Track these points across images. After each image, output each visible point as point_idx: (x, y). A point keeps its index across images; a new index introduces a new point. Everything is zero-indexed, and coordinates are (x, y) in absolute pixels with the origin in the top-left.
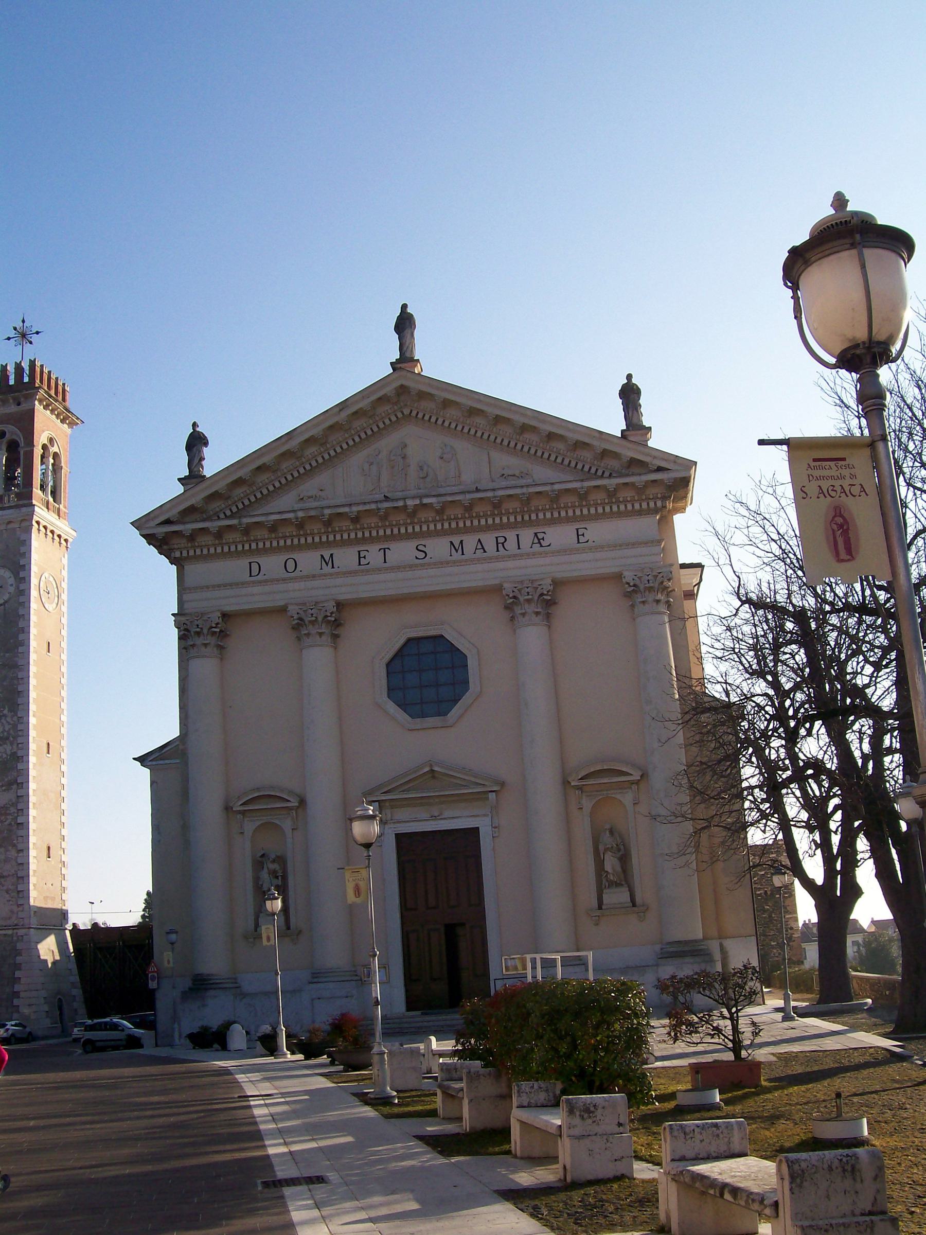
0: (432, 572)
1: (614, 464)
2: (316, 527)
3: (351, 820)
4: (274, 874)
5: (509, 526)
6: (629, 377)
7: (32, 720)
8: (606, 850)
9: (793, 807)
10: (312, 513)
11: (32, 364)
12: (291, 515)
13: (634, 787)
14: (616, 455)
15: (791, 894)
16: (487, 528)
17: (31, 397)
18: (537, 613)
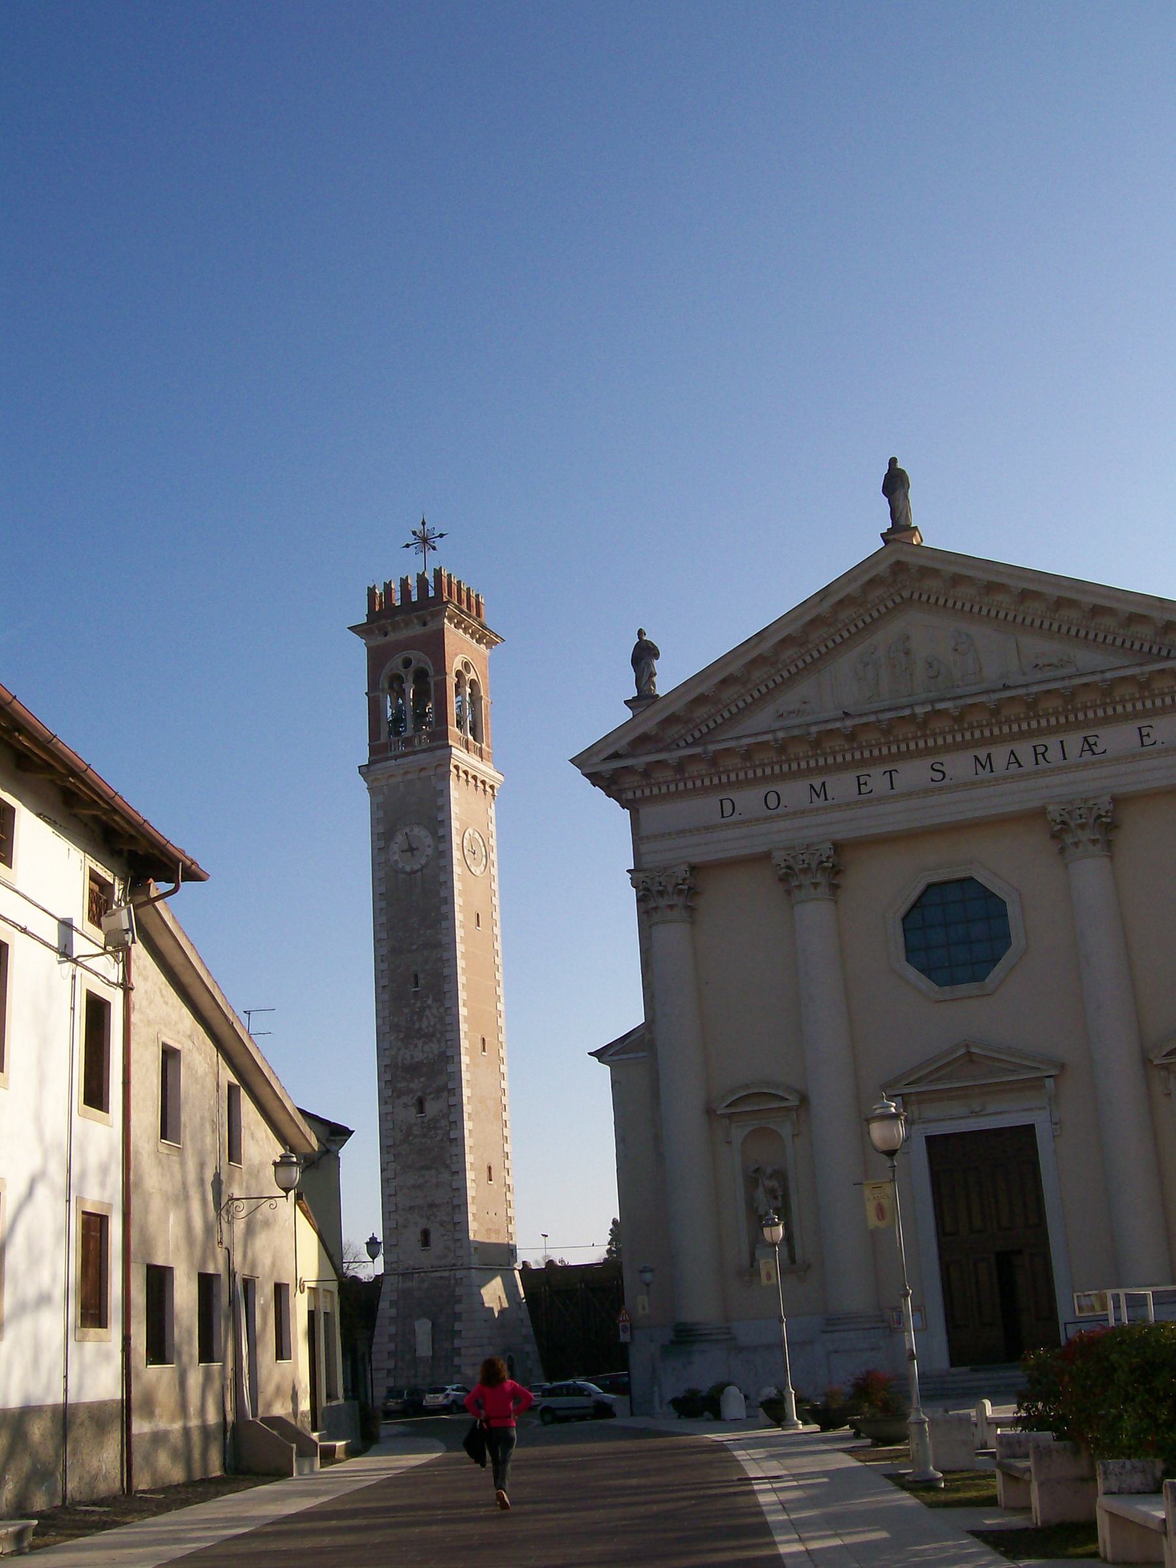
3: (868, 1121)
4: (772, 1193)
5: (1051, 731)
10: (796, 732)
11: (438, 574)
12: (769, 737)
16: (1022, 735)
17: (439, 615)
18: (1094, 842)
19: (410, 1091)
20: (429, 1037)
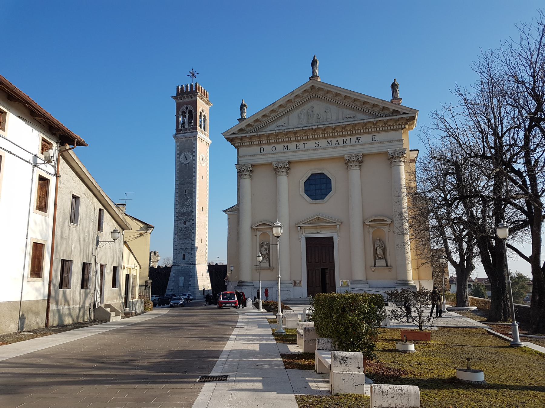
0: (320, 151)
1: (388, 112)
2: (282, 136)
4: (266, 249)
5: (348, 135)
6: (395, 80)
7: (197, 200)
8: (377, 246)
9: (448, 232)
10: (281, 131)
12: (274, 132)
13: (388, 225)
14: (388, 109)
15: (446, 267)
16: (340, 136)
17: (196, 96)
19: (182, 219)
20: (188, 206)
